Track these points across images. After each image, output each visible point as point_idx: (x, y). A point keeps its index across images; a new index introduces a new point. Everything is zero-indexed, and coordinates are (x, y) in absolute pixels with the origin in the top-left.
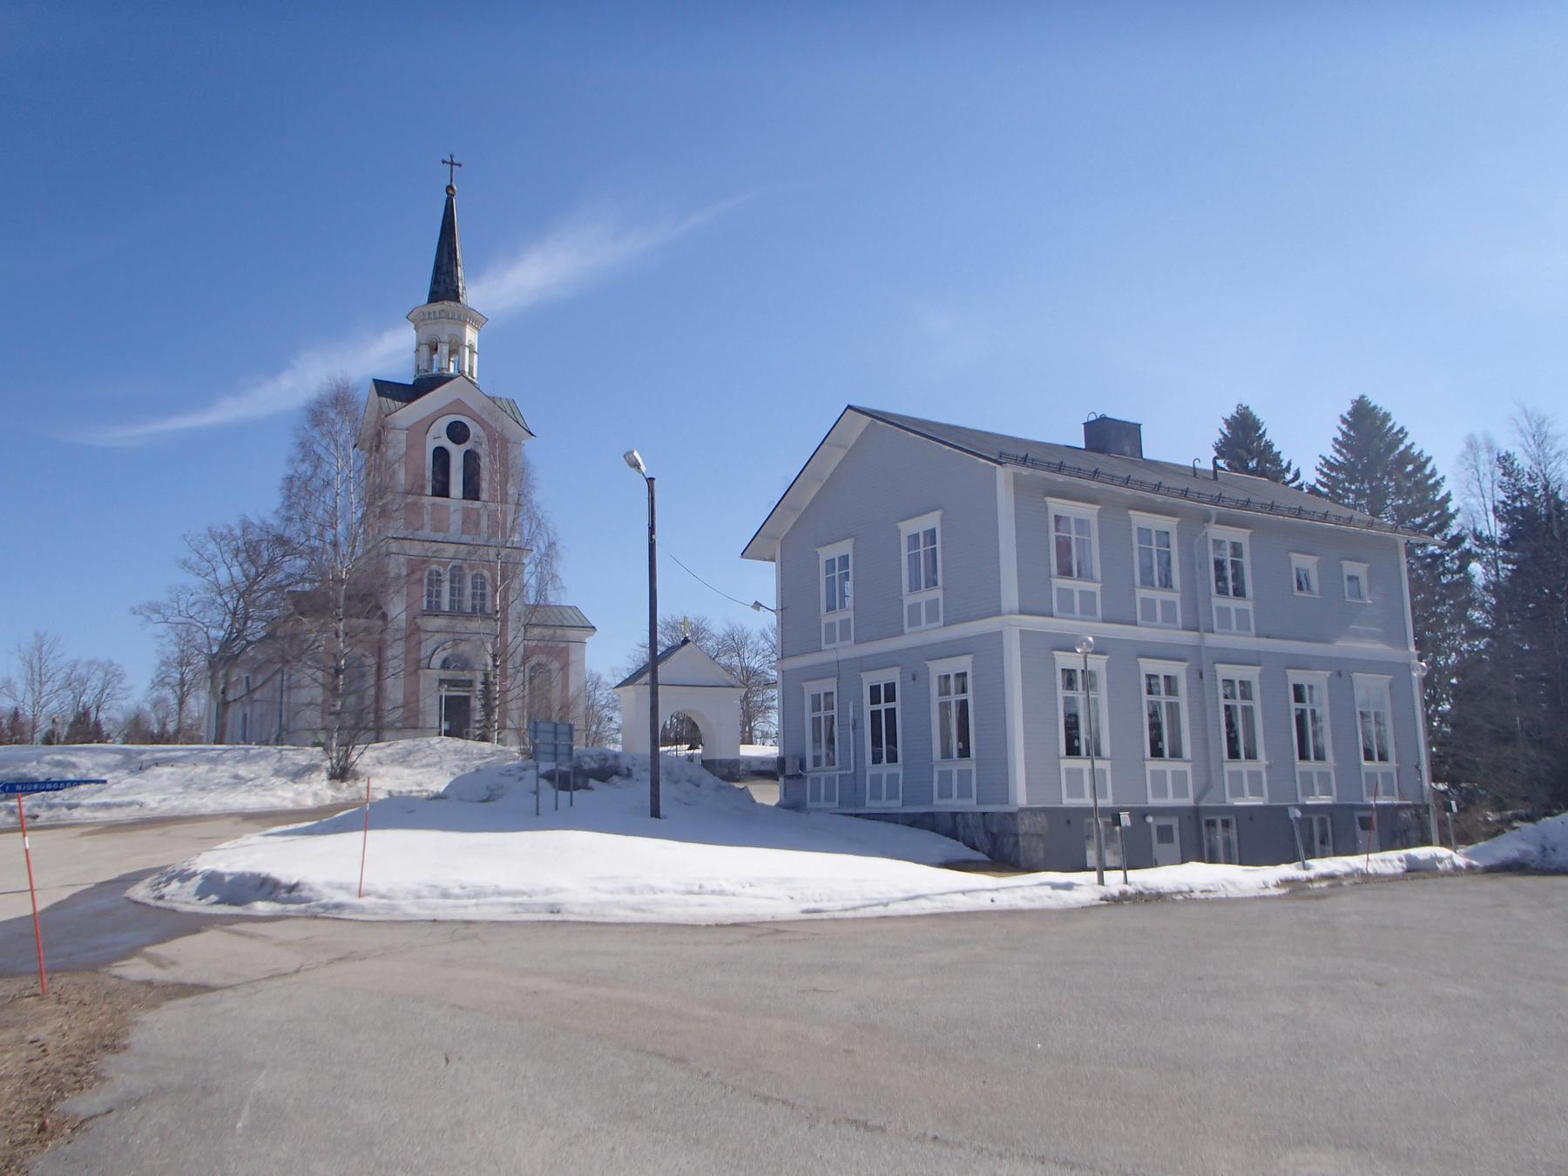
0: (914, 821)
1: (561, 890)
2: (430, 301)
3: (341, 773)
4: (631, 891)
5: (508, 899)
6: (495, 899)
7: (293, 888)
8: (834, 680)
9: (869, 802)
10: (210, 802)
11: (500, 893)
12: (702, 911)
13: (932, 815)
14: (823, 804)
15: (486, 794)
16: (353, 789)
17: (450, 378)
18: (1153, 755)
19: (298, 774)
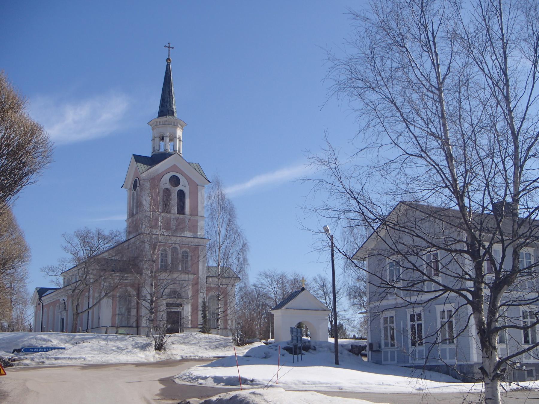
0: (431, 368)
1: (340, 383)
2: (159, 116)
3: (159, 347)
4: (362, 384)
5: (325, 385)
6: (320, 385)
7: (252, 381)
9: (410, 361)
10: (113, 358)
11: (321, 383)
12: (386, 390)
13: (439, 365)
14: (389, 362)
15: (264, 355)
16: (166, 355)
17: (171, 155)
18: (525, 342)
19: (144, 347)
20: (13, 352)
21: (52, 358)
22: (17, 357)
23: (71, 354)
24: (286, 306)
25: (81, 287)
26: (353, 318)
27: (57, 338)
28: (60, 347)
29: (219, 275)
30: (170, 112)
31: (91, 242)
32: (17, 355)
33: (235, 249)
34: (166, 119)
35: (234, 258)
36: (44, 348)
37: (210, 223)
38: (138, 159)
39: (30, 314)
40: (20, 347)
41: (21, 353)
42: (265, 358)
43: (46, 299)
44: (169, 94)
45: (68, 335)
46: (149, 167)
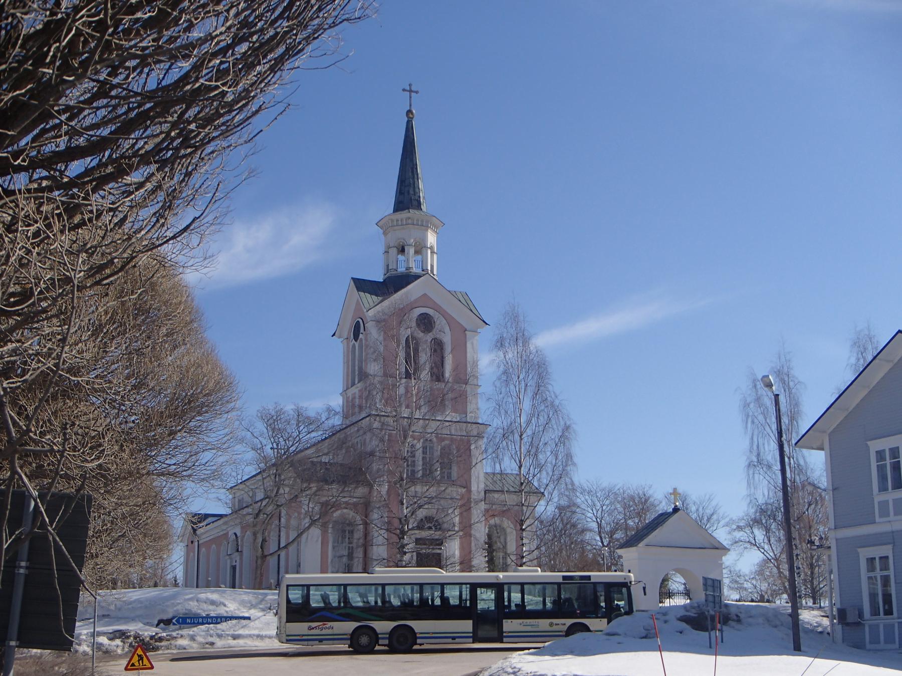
2: (394, 211)
8: (890, 547)
14: (882, 645)
15: (644, 633)
17: (417, 277)
20: (157, 625)
21: (228, 635)
22: (165, 634)
23: (262, 629)
24: (646, 541)
25: (270, 509)
26: (745, 565)
27: (234, 600)
28: (241, 615)
29: (522, 484)
30: (415, 203)
31: (285, 429)
32: (164, 630)
33: (552, 435)
34: (408, 215)
35: (549, 453)
36: (212, 617)
37: (503, 390)
38: (361, 285)
39: (176, 560)
40: (170, 616)
41: (172, 627)
42: (645, 637)
43: (206, 532)
44: (413, 172)
45: (255, 593)
46: (380, 298)
